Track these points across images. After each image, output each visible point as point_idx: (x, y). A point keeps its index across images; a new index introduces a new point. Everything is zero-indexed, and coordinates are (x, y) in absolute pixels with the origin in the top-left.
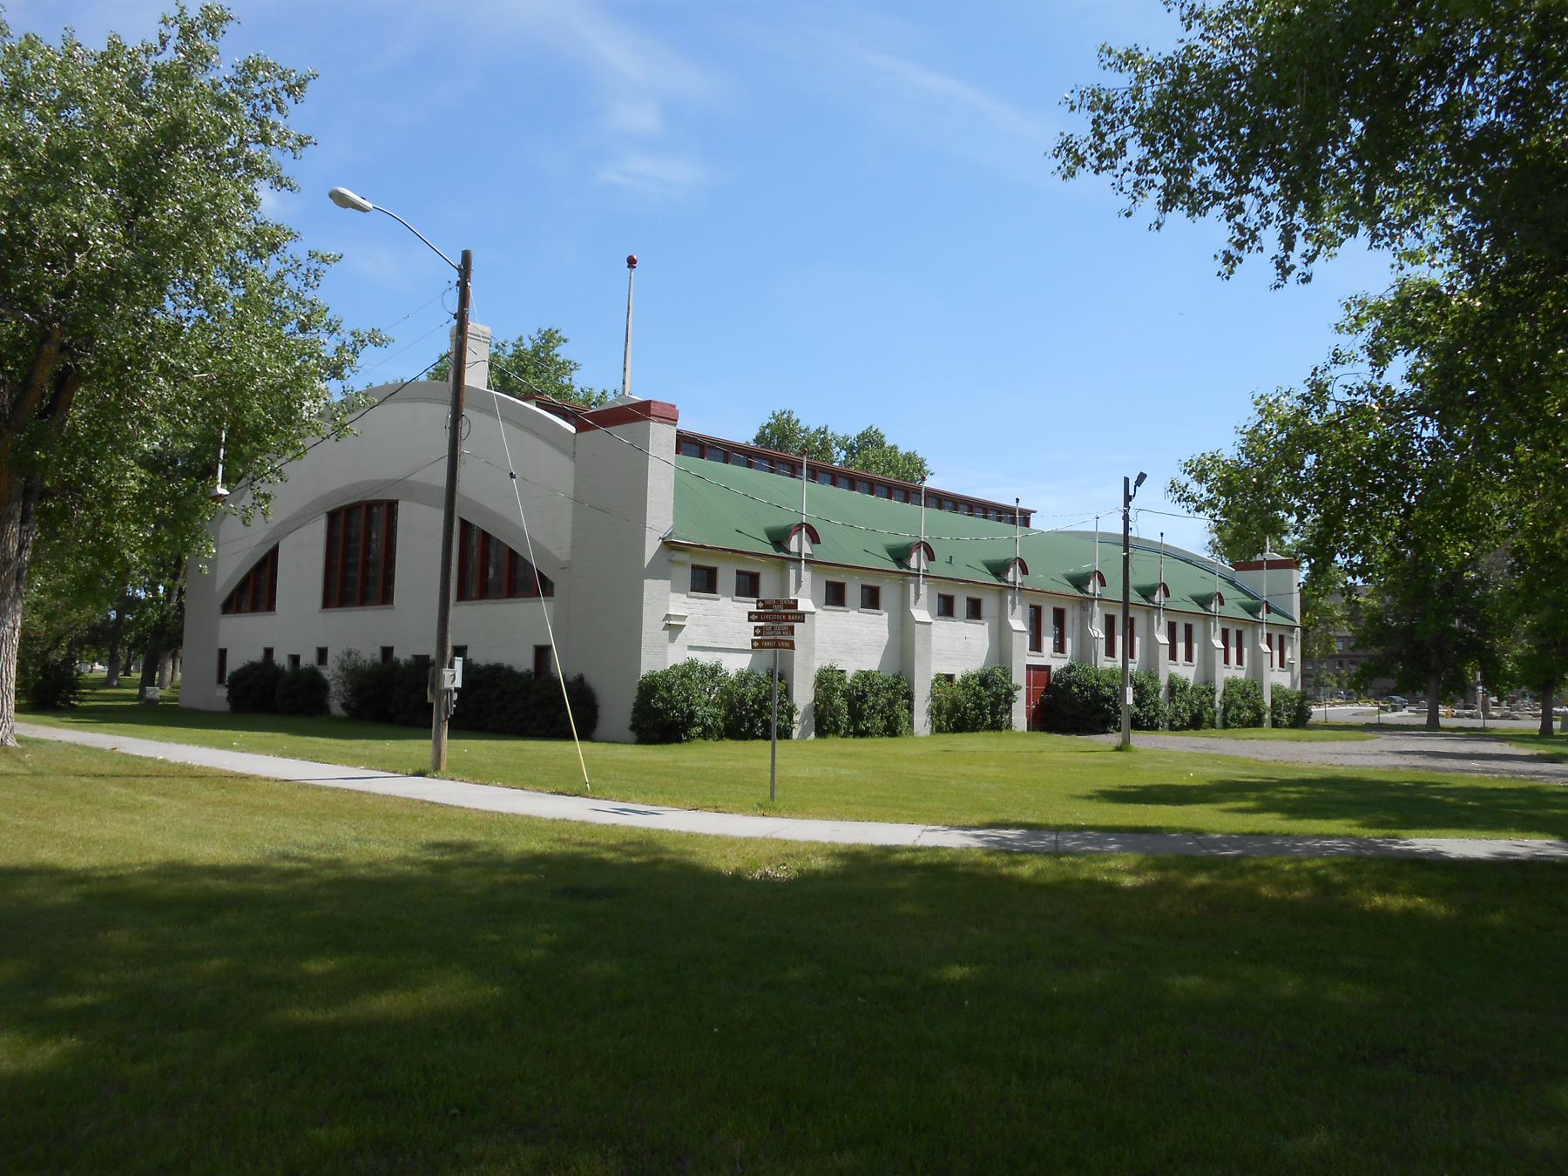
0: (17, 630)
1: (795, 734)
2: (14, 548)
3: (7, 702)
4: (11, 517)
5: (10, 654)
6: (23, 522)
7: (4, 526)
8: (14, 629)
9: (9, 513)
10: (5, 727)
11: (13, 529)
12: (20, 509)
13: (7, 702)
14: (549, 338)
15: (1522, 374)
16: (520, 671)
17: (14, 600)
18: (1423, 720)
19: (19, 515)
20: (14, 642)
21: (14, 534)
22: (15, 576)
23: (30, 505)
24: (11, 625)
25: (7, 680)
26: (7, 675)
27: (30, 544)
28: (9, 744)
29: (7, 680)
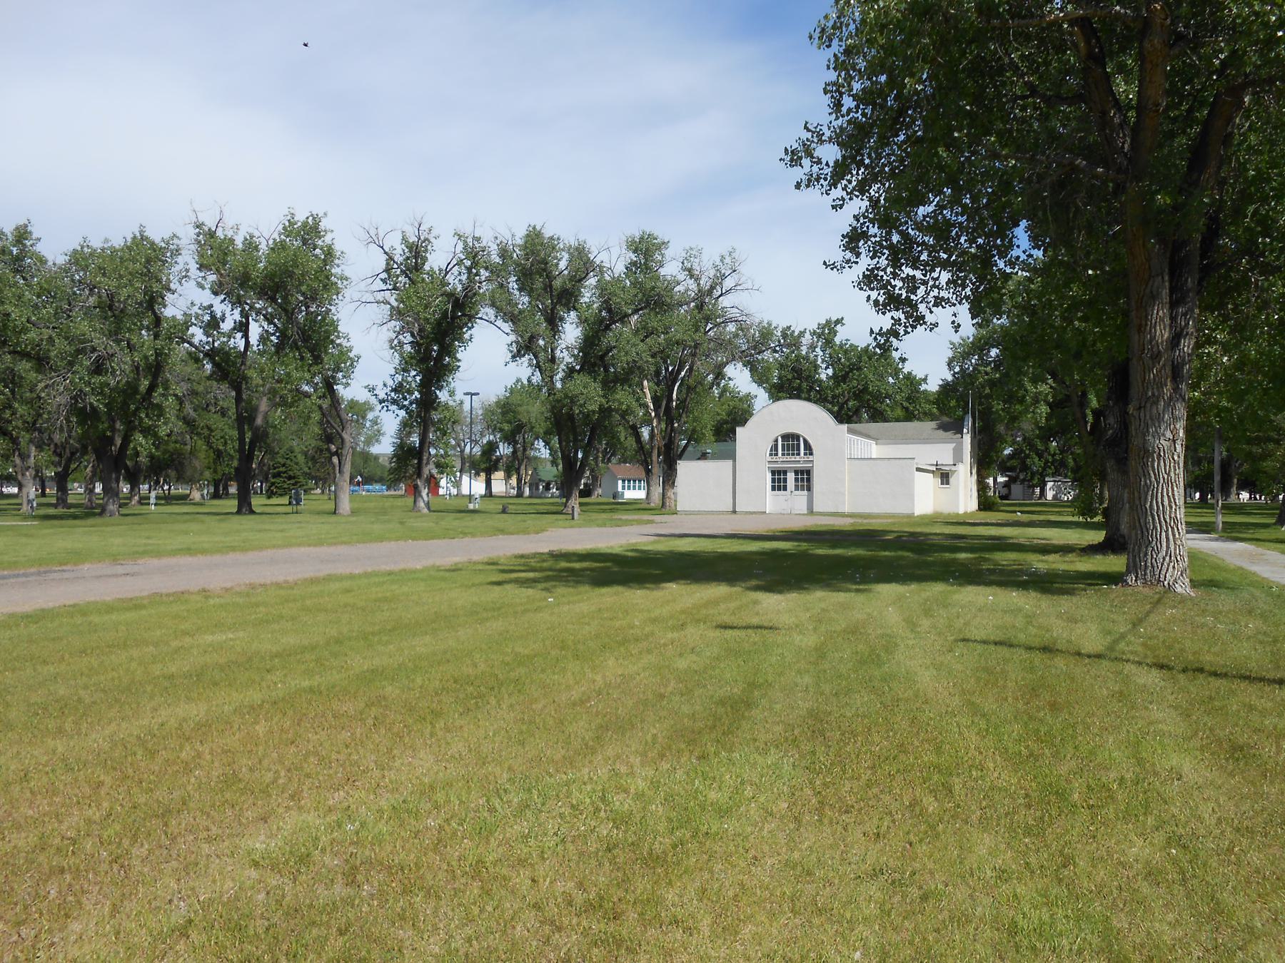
0: (1179, 442)
1: (780, 439)
2: (1162, 336)
3: (1174, 535)
4: (1154, 297)
5: (1172, 475)
6: (1173, 305)
7: (1146, 310)
8: (1174, 441)
9: (1152, 292)
10: (1174, 567)
11: (1160, 312)
12: (1167, 284)
13: (1174, 535)
14: (665, 244)
15: (970, 157)
16: (118, 242)
17: (1170, 403)
18: (1098, 537)
19: (1165, 293)
20: (1176, 458)
21: (1162, 320)
22: (1170, 373)
23: (1186, 280)
24: (1169, 435)
25: (1171, 507)
26: (1170, 501)
27: (1191, 330)
28: (1179, 590)
29: (1171, 507)
